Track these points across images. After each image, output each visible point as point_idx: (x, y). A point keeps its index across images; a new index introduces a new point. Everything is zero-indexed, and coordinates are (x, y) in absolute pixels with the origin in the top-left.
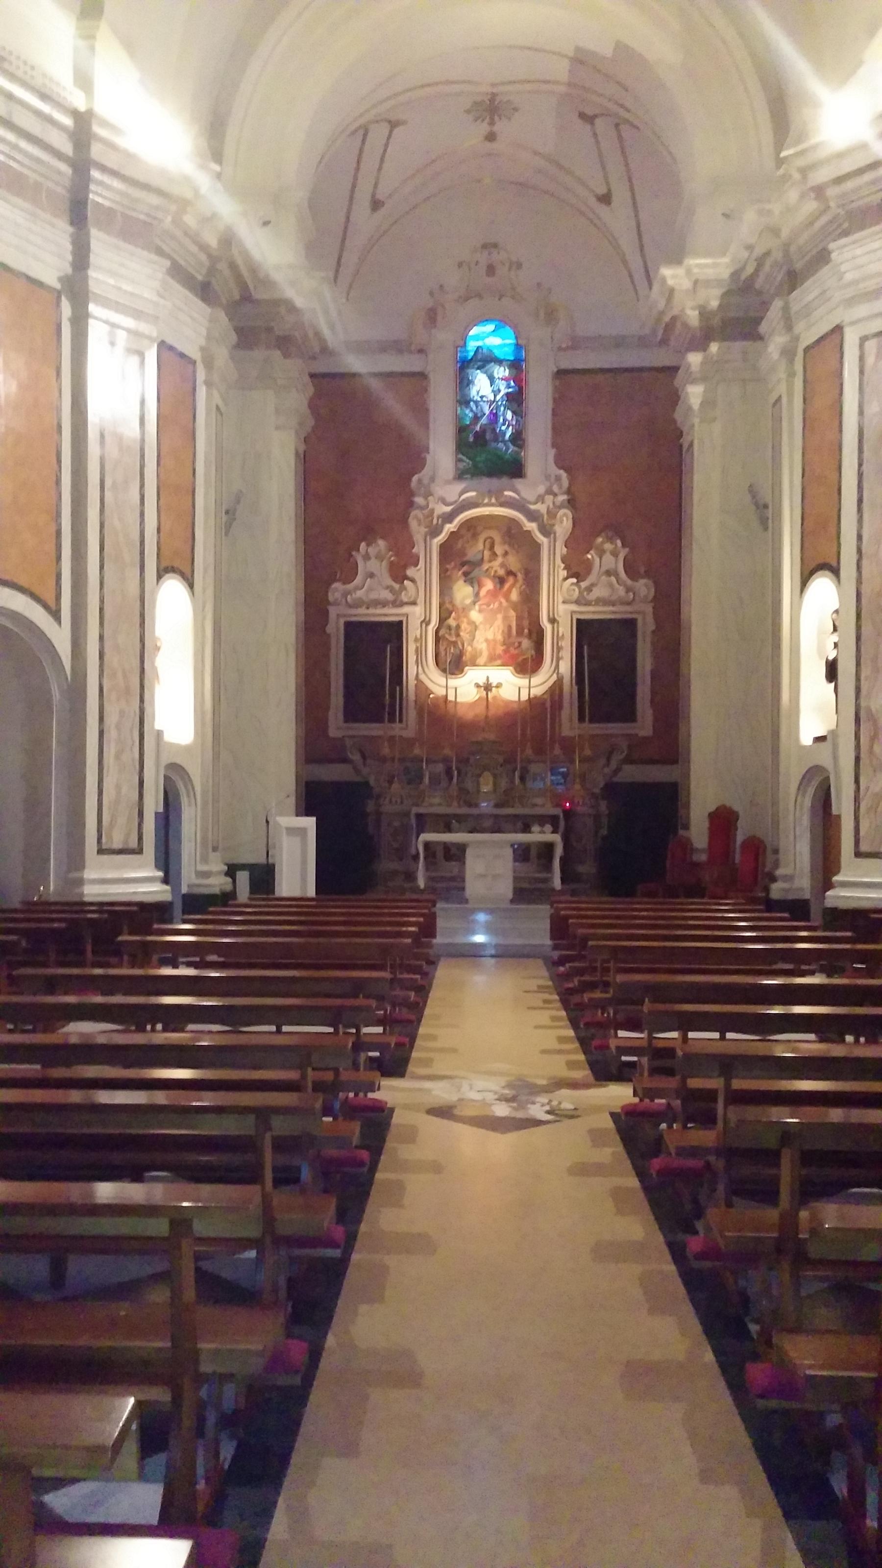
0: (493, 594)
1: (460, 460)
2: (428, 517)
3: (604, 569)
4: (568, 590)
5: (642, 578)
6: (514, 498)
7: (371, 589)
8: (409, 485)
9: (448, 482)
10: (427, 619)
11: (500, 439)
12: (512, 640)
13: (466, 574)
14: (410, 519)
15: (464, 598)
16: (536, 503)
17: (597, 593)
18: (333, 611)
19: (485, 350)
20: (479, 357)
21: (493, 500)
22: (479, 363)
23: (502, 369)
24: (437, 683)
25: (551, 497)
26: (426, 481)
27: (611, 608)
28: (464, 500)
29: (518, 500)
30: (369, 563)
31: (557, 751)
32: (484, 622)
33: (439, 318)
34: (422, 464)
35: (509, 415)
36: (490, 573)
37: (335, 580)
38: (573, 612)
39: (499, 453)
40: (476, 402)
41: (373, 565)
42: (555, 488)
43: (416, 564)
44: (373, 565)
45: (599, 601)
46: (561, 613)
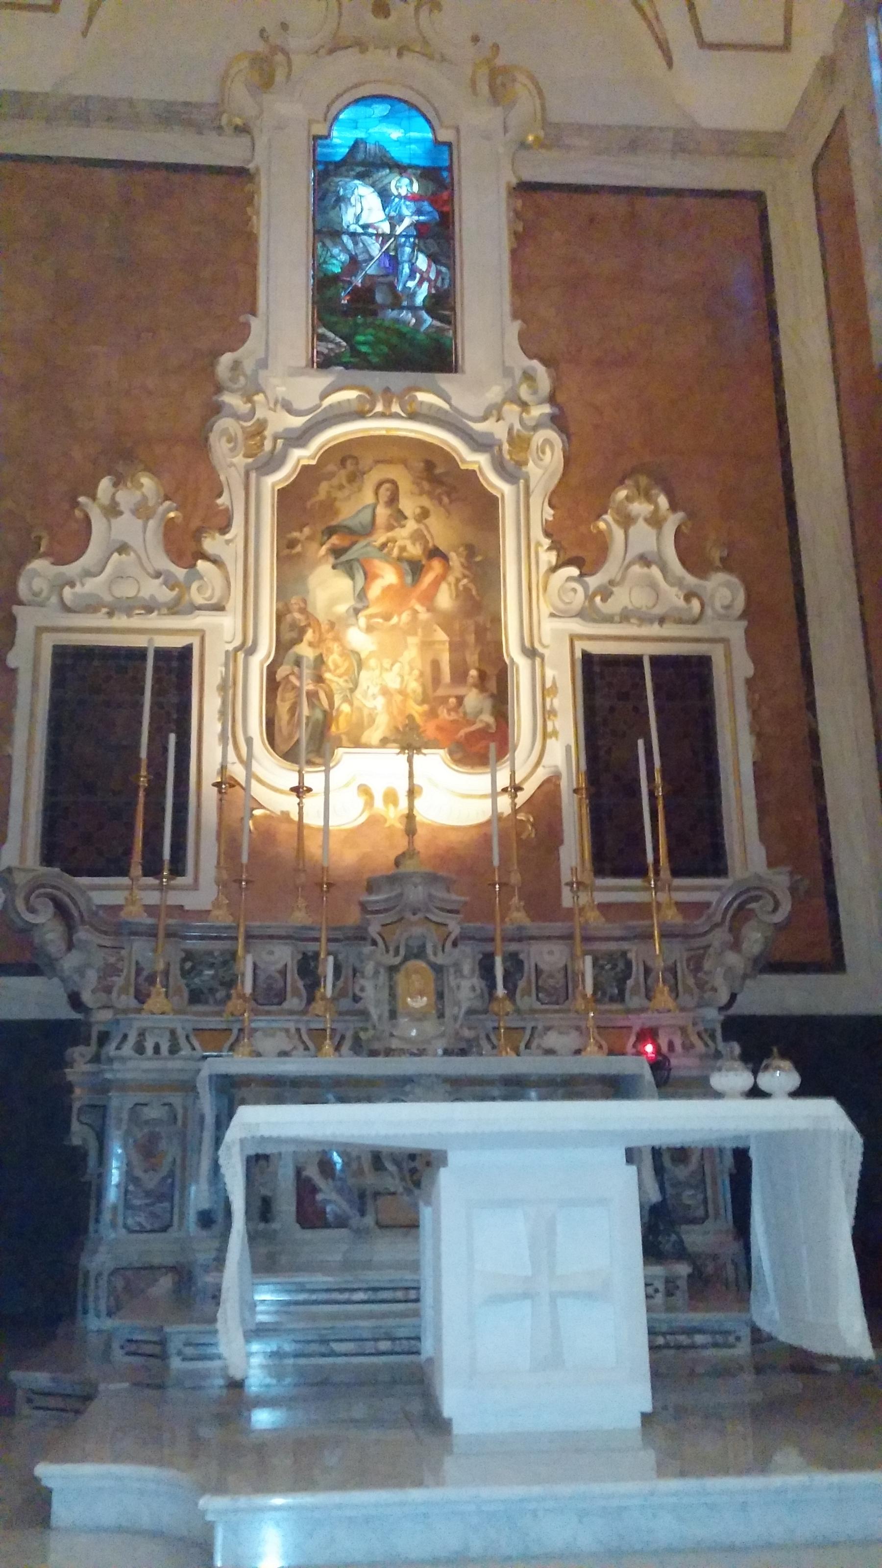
0: (398, 596)
1: (322, 338)
2: (252, 436)
3: (633, 553)
4: (562, 590)
5: (717, 569)
6: (440, 409)
7: (120, 576)
8: (213, 373)
9: (296, 372)
10: (249, 643)
11: (405, 303)
12: (441, 692)
13: (337, 552)
14: (213, 437)
15: (333, 602)
16: (484, 418)
17: (621, 599)
18: (27, 620)
19: (371, 147)
20: (360, 156)
21: (396, 408)
22: (360, 169)
23: (405, 181)
24: (272, 784)
25: (516, 408)
26: (248, 366)
27: (655, 630)
28: (331, 406)
29: (446, 412)
30: (117, 522)
31: (547, 956)
32: (379, 649)
33: (280, 76)
34: (241, 335)
35: (422, 262)
36: (390, 553)
37: (33, 552)
38: (573, 639)
39: (405, 330)
40: (353, 235)
41: (126, 527)
42: (524, 392)
43: (224, 529)
44: (126, 527)
45: (625, 617)
46: (546, 640)
